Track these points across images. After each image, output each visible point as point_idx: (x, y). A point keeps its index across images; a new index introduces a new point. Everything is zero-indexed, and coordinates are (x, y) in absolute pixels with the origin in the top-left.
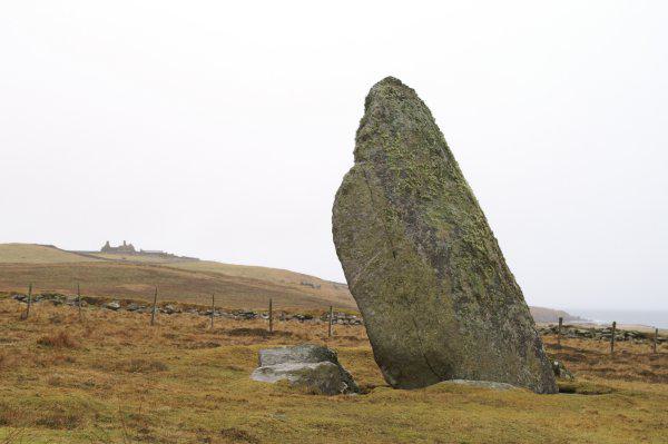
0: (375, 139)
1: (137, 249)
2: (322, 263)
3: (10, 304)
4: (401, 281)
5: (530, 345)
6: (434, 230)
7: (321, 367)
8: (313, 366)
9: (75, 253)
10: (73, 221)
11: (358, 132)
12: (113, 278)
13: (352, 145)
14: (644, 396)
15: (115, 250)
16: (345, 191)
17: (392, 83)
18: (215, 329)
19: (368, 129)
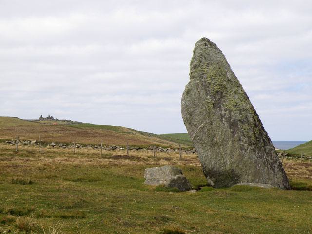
0: (199, 68)
1: (55, 118)
2: (181, 128)
3: (311, 177)
4: (215, 136)
5: (277, 165)
6: (230, 111)
7: (179, 177)
8: (176, 177)
9: (27, 120)
10: (26, 103)
11: (191, 65)
12: (45, 132)
13: (188, 71)
14: (59, 154)
15: (44, 119)
16: (188, 92)
17: (206, 43)
18: (75, 152)
19: (196, 62)
